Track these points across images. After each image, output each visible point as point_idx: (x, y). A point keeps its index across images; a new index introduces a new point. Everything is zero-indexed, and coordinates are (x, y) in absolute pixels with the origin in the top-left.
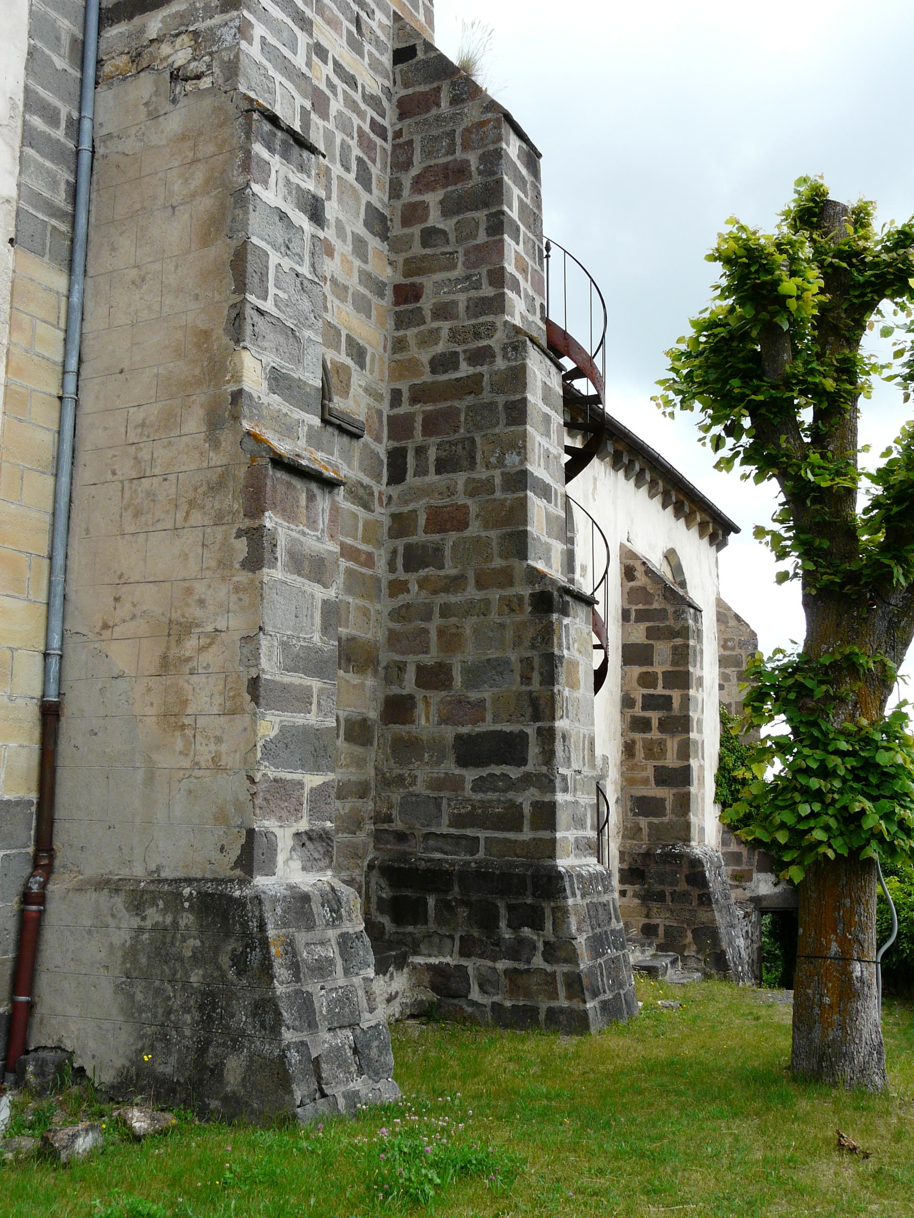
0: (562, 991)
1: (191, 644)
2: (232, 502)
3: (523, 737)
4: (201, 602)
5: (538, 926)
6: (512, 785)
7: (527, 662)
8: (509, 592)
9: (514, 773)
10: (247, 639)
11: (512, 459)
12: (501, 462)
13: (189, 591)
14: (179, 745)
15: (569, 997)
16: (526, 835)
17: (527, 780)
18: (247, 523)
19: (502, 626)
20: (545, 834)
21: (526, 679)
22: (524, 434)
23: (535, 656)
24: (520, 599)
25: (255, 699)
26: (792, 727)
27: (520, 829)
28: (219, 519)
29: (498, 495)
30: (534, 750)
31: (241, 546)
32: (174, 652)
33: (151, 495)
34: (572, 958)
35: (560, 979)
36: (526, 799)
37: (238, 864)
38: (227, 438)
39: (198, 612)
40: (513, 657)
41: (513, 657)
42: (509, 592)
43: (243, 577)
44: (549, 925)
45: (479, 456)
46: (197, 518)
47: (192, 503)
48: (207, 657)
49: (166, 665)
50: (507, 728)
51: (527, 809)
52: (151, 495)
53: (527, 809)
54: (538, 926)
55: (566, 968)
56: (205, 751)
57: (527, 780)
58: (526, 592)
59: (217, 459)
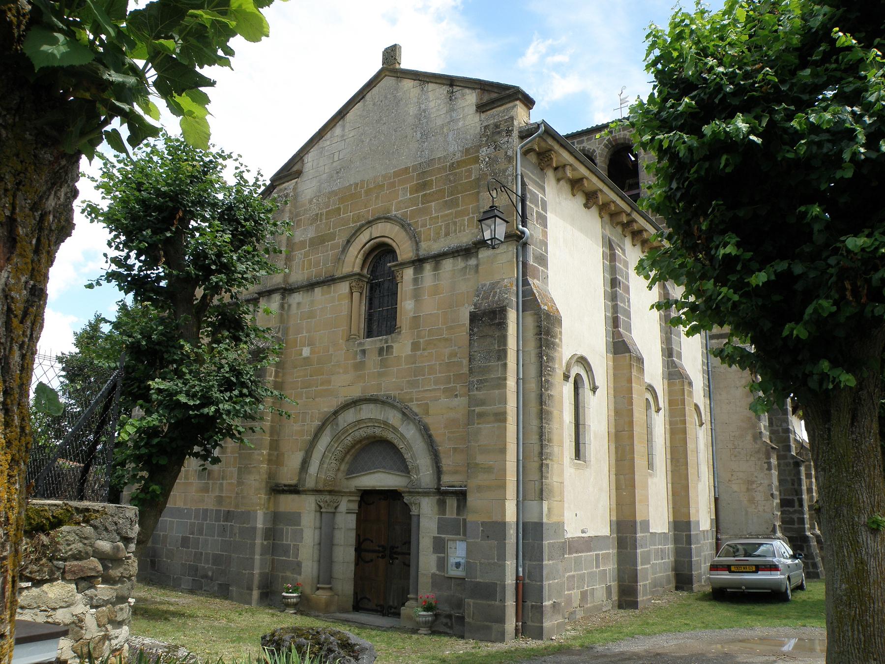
0: (811, 567)
1: (754, 486)
2: (762, 456)
3: (793, 500)
4: (756, 477)
5: (802, 550)
6: (790, 513)
7: (793, 480)
8: (787, 461)
9: (791, 509)
10: (769, 485)
11: (784, 425)
12: (781, 425)
13: (753, 474)
14: (754, 507)
15: (813, 568)
16: (796, 526)
17: (795, 512)
18: (766, 461)
19: (785, 470)
20: (802, 526)
21: (793, 485)
22: (788, 418)
23: (795, 478)
24: (790, 463)
25: (773, 498)
26: (119, 318)
27: (794, 524)
28: (759, 459)
29: (781, 434)
30: (797, 504)
31: (766, 466)
32: (750, 487)
33: (739, 453)
34: (813, 558)
35: (810, 564)
36: (795, 517)
37: (772, 531)
38: (759, 442)
39: (756, 479)
40: (789, 478)
41: (789, 478)
42: (787, 461)
43: (767, 472)
44: (805, 549)
45: (774, 423)
46: (753, 459)
47: (751, 455)
48: (759, 488)
49: (748, 490)
50: (788, 498)
51: (796, 520)
52: (739, 453)
53: (796, 520)
54: (802, 550)
55: (811, 561)
56: (761, 508)
57: (795, 512)
58: (791, 461)
59: (757, 446)
